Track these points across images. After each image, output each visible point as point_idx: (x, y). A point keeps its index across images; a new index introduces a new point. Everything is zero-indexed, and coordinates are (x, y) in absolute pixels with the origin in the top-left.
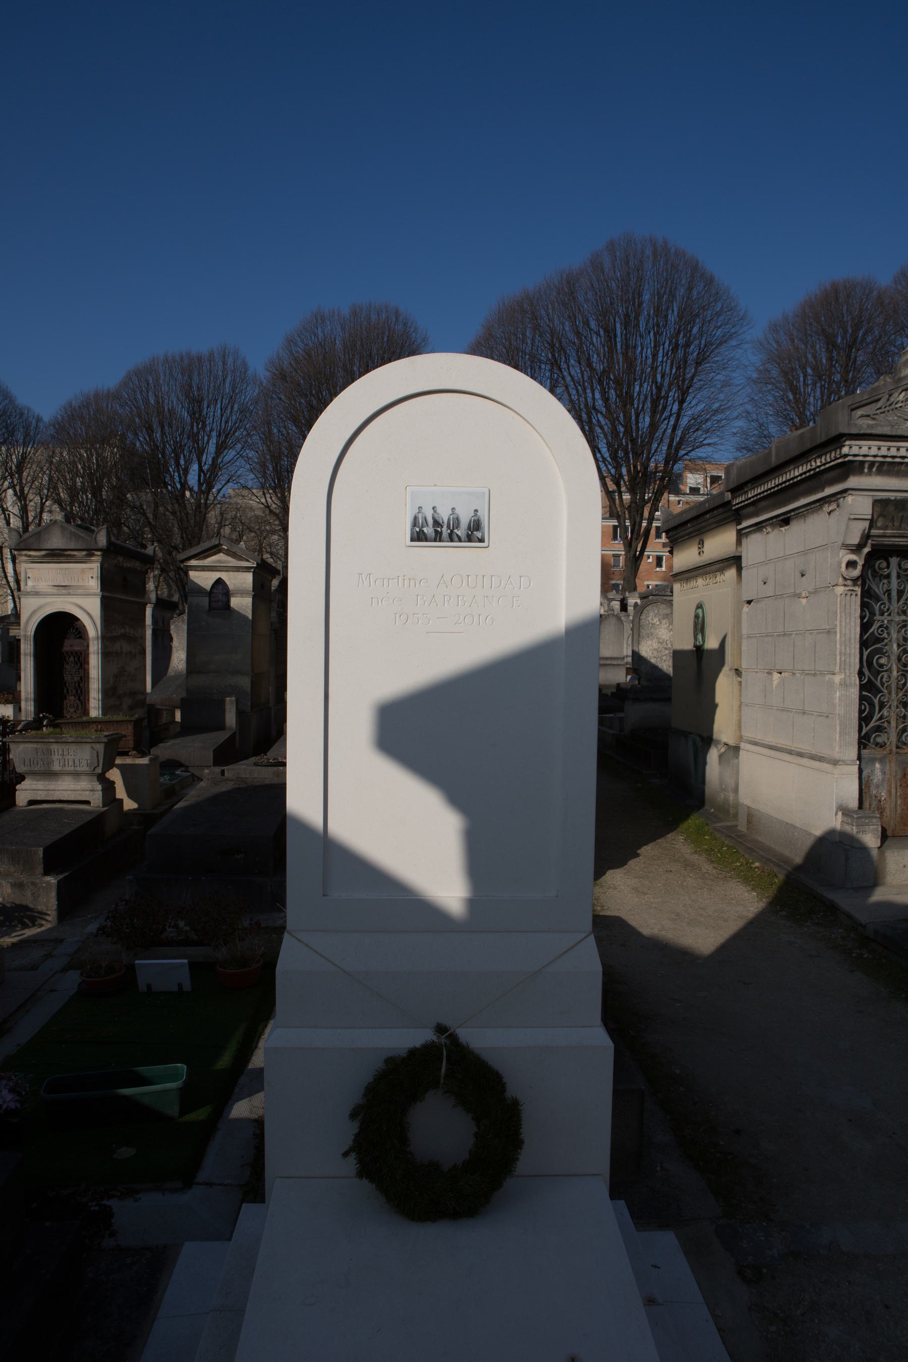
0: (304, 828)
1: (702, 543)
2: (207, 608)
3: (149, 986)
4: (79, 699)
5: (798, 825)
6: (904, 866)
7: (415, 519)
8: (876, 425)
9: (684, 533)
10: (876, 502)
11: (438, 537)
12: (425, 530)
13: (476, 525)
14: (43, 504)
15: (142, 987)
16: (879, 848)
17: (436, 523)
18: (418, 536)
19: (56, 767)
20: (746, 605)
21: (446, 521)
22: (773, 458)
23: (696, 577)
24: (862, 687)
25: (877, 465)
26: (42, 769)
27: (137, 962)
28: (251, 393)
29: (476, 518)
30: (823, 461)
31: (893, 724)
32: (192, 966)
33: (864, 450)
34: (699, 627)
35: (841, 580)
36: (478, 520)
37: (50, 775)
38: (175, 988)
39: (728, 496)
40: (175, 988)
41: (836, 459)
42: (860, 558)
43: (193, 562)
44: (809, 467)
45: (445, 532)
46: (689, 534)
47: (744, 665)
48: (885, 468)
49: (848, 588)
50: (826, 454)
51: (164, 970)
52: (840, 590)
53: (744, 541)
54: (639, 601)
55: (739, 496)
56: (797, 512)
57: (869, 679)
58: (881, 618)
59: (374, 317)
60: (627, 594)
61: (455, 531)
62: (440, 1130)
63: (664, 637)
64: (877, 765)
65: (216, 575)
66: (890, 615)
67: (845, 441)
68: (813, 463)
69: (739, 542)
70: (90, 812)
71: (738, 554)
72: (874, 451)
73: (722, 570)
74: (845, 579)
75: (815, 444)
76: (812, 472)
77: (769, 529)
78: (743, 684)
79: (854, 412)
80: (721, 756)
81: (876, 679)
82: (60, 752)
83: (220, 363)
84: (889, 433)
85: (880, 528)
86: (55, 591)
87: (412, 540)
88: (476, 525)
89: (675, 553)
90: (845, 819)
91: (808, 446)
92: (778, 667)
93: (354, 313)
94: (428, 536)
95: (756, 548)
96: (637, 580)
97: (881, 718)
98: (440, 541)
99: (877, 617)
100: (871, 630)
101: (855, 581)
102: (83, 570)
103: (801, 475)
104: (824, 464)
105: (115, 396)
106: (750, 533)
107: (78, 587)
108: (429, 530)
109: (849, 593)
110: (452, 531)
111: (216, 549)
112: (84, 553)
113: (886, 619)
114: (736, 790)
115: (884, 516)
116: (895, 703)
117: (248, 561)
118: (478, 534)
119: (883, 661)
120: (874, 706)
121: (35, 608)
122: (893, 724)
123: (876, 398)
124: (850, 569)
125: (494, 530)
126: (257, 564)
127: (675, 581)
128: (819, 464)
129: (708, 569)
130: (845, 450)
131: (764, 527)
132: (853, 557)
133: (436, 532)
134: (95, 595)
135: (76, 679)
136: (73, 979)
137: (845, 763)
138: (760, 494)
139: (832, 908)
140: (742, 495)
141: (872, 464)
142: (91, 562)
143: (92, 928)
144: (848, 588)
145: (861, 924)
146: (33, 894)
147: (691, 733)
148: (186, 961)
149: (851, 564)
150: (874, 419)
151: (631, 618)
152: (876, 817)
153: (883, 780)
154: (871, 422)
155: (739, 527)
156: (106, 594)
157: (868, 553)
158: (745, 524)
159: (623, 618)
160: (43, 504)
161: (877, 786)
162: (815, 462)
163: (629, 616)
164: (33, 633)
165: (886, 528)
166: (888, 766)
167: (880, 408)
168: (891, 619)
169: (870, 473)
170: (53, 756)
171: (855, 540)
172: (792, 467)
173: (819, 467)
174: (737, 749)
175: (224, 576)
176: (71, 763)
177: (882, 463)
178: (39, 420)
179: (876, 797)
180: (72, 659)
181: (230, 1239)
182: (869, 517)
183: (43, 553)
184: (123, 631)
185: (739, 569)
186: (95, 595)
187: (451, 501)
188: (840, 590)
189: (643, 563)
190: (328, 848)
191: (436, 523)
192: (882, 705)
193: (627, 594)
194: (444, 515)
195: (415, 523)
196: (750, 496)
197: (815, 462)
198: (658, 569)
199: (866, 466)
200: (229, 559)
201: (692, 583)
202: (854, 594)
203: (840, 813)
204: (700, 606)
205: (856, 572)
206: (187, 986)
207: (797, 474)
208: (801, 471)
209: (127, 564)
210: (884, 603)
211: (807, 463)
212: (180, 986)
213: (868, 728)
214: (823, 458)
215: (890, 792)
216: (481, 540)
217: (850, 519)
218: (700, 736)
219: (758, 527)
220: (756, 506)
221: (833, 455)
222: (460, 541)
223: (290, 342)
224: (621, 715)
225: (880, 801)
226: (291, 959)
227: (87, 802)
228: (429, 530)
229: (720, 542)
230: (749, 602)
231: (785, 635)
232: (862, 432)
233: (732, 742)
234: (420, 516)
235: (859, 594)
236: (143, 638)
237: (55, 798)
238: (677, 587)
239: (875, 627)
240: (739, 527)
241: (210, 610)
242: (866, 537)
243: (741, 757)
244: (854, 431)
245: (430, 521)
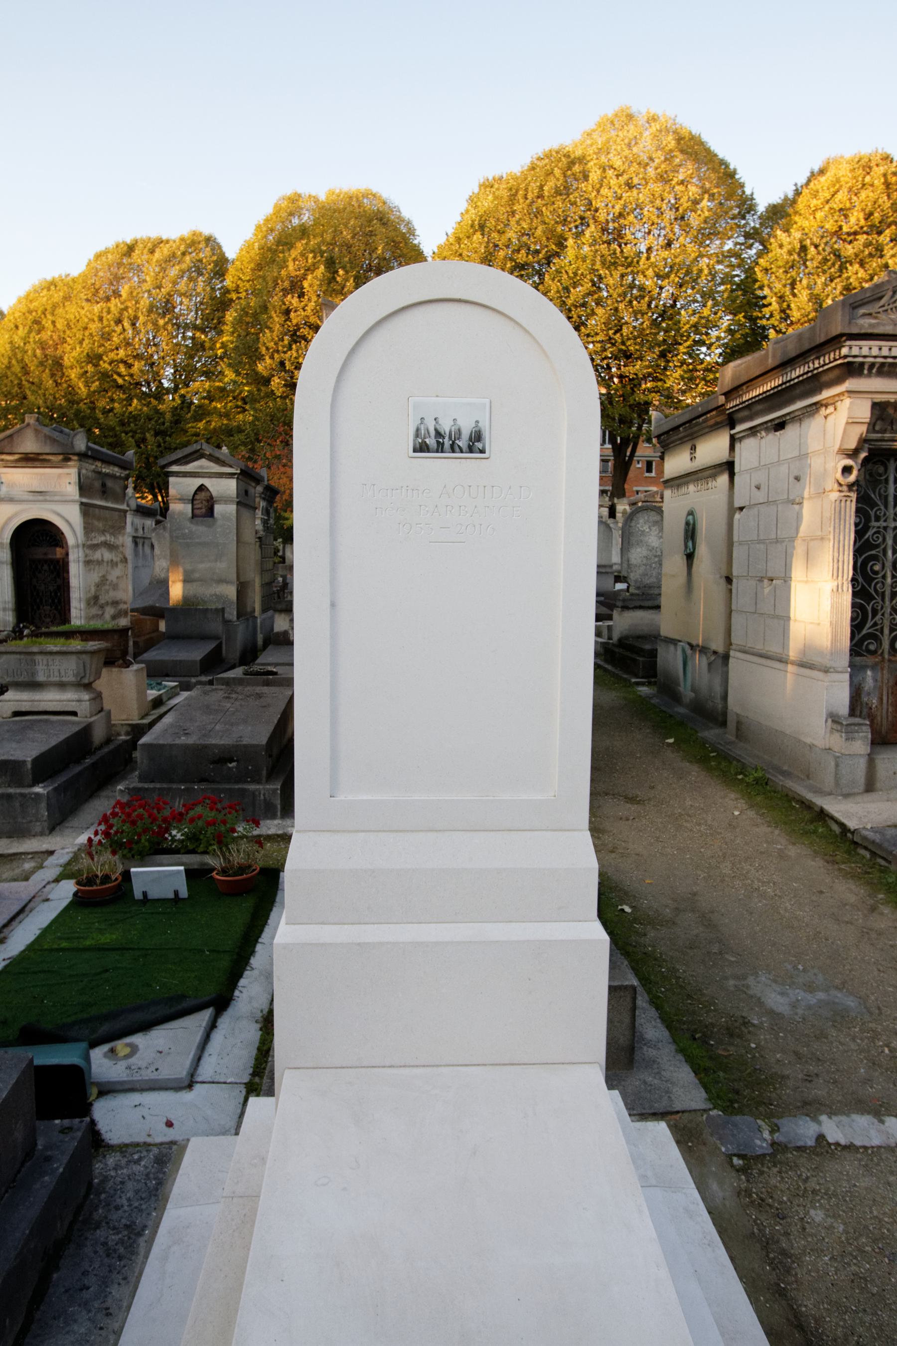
1: (694, 448)
2: (190, 515)
3: (145, 894)
4: (56, 609)
5: (787, 732)
6: (895, 773)
7: (418, 430)
8: (878, 324)
9: (676, 437)
10: (875, 405)
11: (440, 448)
12: (427, 441)
15: (138, 895)
16: (869, 755)
17: (438, 434)
18: (422, 448)
19: (41, 678)
20: (738, 512)
21: (448, 433)
22: (770, 361)
23: (687, 483)
24: (855, 594)
25: (877, 366)
26: (26, 679)
27: (133, 870)
29: (477, 429)
30: (822, 362)
31: (886, 631)
32: (188, 872)
33: (865, 351)
34: (690, 533)
35: (836, 486)
36: (480, 431)
37: (34, 685)
38: (171, 896)
39: (722, 399)
40: (172, 896)
41: (835, 360)
42: (856, 463)
43: (175, 468)
44: (806, 369)
45: (447, 443)
46: (680, 439)
47: (735, 573)
48: (886, 369)
49: (843, 494)
50: (824, 355)
51: (160, 877)
52: (835, 495)
53: (737, 446)
54: (627, 508)
55: (733, 400)
56: (792, 416)
57: (863, 586)
58: (877, 524)
60: (616, 500)
61: (457, 442)
63: (653, 544)
64: (869, 673)
65: (198, 482)
66: (885, 521)
67: (845, 341)
68: (811, 365)
69: (732, 448)
70: (78, 723)
71: (731, 459)
72: (875, 351)
73: (714, 476)
74: (840, 485)
75: (813, 345)
76: (810, 374)
77: (763, 433)
78: (734, 591)
79: (856, 311)
80: (710, 664)
81: (870, 587)
82: (45, 662)
84: (891, 332)
85: (878, 432)
86: (31, 497)
87: (415, 451)
88: (477, 436)
89: (666, 459)
90: (835, 726)
91: (807, 346)
92: (770, 575)
94: (431, 447)
95: (749, 453)
96: (626, 486)
97: (875, 624)
98: (442, 452)
99: (874, 523)
100: (866, 537)
101: (850, 487)
102: (60, 475)
103: (798, 377)
104: (823, 366)
106: (743, 437)
107: (55, 494)
108: (431, 441)
109: (845, 498)
110: (453, 442)
111: (198, 455)
112: (61, 457)
113: (882, 524)
114: (725, 697)
115: (883, 420)
116: (889, 610)
117: (231, 466)
118: (479, 445)
119: (877, 568)
120: (867, 614)
121: (9, 515)
122: (886, 631)
123: (879, 295)
124: (846, 474)
125: (491, 442)
126: (241, 470)
127: (666, 487)
128: (817, 365)
129: (700, 475)
130: (845, 351)
131: (758, 431)
132: (849, 462)
133: (438, 442)
134: (73, 501)
135: (51, 588)
136: (68, 888)
138: (756, 397)
139: (822, 815)
140: (736, 398)
141: (872, 365)
142: (68, 467)
143: (83, 839)
144: (843, 494)
145: (849, 830)
146: (21, 805)
147: (680, 641)
148: (182, 868)
149: (847, 470)
150: (876, 318)
151: (620, 525)
152: (866, 725)
153: (875, 687)
154: (873, 321)
155: (733, 432)
156: (84, 500)
157: (865, 458)
158: (739, 428)
159: (611, 525)
161: (869, 694)
162: (813, 363)
163: (617, 522)
164: (9, 541)
165: (883, 431)
166: (879, 674)
167: (883, 306)
168: (890, 520)
169: (870, 375)
170: (37, 667)
171: (852, 444)
172: (789, 369)
173: (817, 368)
174: (726, 658)
175: (207, 482)
176: (56, 674)
177: (883, 364)
179: (867, 704)
180: (46, 567)
181: (237, 1134)
182: (868, 420)
183: (16, 457)
184: (103, 539)
185: (732, 475)
186: (73, 501)
187: (459, 417)
189: (632, 468)
191: (438, 434)
192: (875, 612)
193: (616, 500)
194: (446, 427)
195: (417, 433)
196: (744, 399)
197: (813, 363)
198: (647, 475)
199: (866, 367)
200: (212, 464)
201: (684, 490)
202: (849, 499)
203: (830, 721)
204: (691, 513)
205: (852, 478)
206: (184, 893)
207: (793, 376)
208: (798, 373)
209: (106, 470)
210: (880, 509)
211: (804, 365)
212: (176, 893)
213: (860, 636)
214: (822, 359)
215: (881, 699)
216: (482, 451)
217: (847, 423)
218: (689, 644)
219: (753, 431)
220: (752, 408)
221: (832, 355)
222: (462, 452)
224: (610, 623)
225: (871, 708)
226: (301, 861)
227: (74, 714)
228: (431, 441)
229: (713, 448)
230: (741, 509)
231: (777, 542)
232: (863, 331)
233: (721, 649)
234: (422, 427)
235: (854, 500)
237: (40, 709)
238: (667, 493)
239: (870, 533)
240: (733, 432)
241: (192, 518)
242: (863, 441)
243: (730, 665)
244: (855, 330)
245: (433, 433)
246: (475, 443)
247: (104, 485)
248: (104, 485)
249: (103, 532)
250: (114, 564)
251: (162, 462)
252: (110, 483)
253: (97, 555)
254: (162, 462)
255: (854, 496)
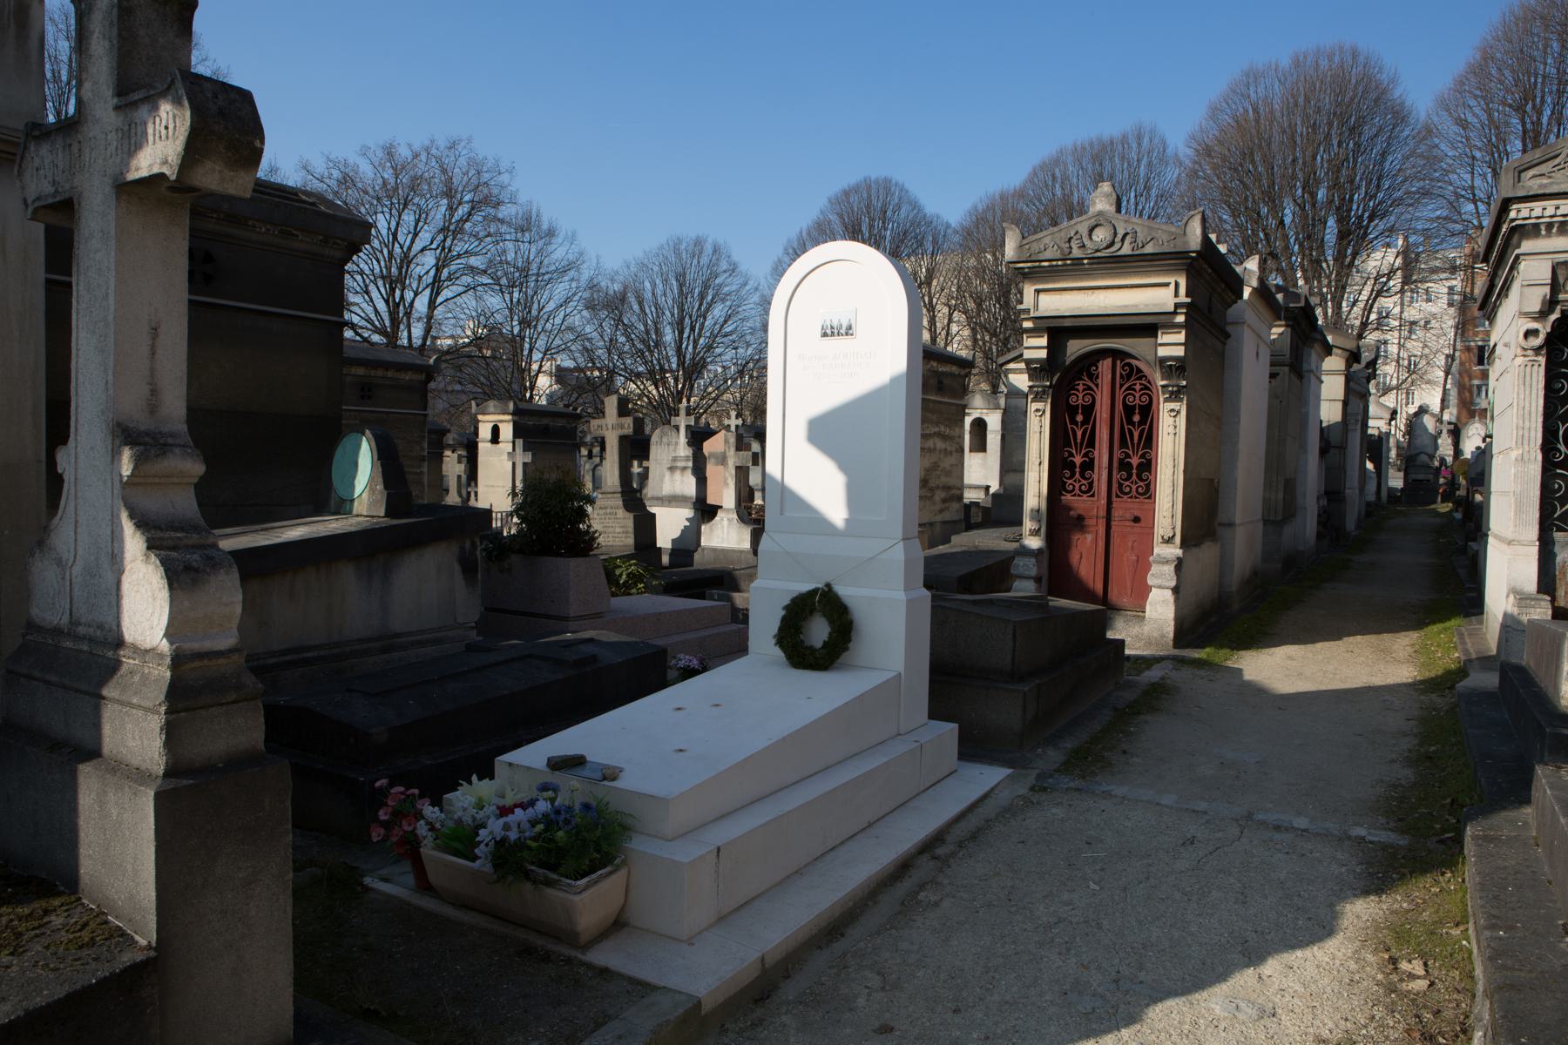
0: (773, 479)
13: (850, 328)
14: (950, 315)
18: (825, 335)
28: (1172, 174)
43: (1012, 366)
59: (1324, 64)
62: (818, 631)
83: (1134, 145)
88: (850, 328)
93: (1297, 63)
101: (1537, 350)
105: (1020, 194)
125: (858, 330)
132: (1535, 325)
137: (1520, 543)
141: (1550, 226)
149: (1529, 334)
160: (950, 315)
178: (948, 226)
187: (839, 317)
188: (1520, 360)
190: (783, 489)
194: (835, 324)
205: (1537, 341)
209: (942, 369)
223: (1214, 111)
236: (962, 437)
246: (849, 331)
247: (940, 382)
248: (940, 382)
249: (937, 424)
250: (946, 452)
251: (1001, 360)
252: (946, 381)
253: (930, 443)
254: (1001, 360)
255: (1542, 360)
